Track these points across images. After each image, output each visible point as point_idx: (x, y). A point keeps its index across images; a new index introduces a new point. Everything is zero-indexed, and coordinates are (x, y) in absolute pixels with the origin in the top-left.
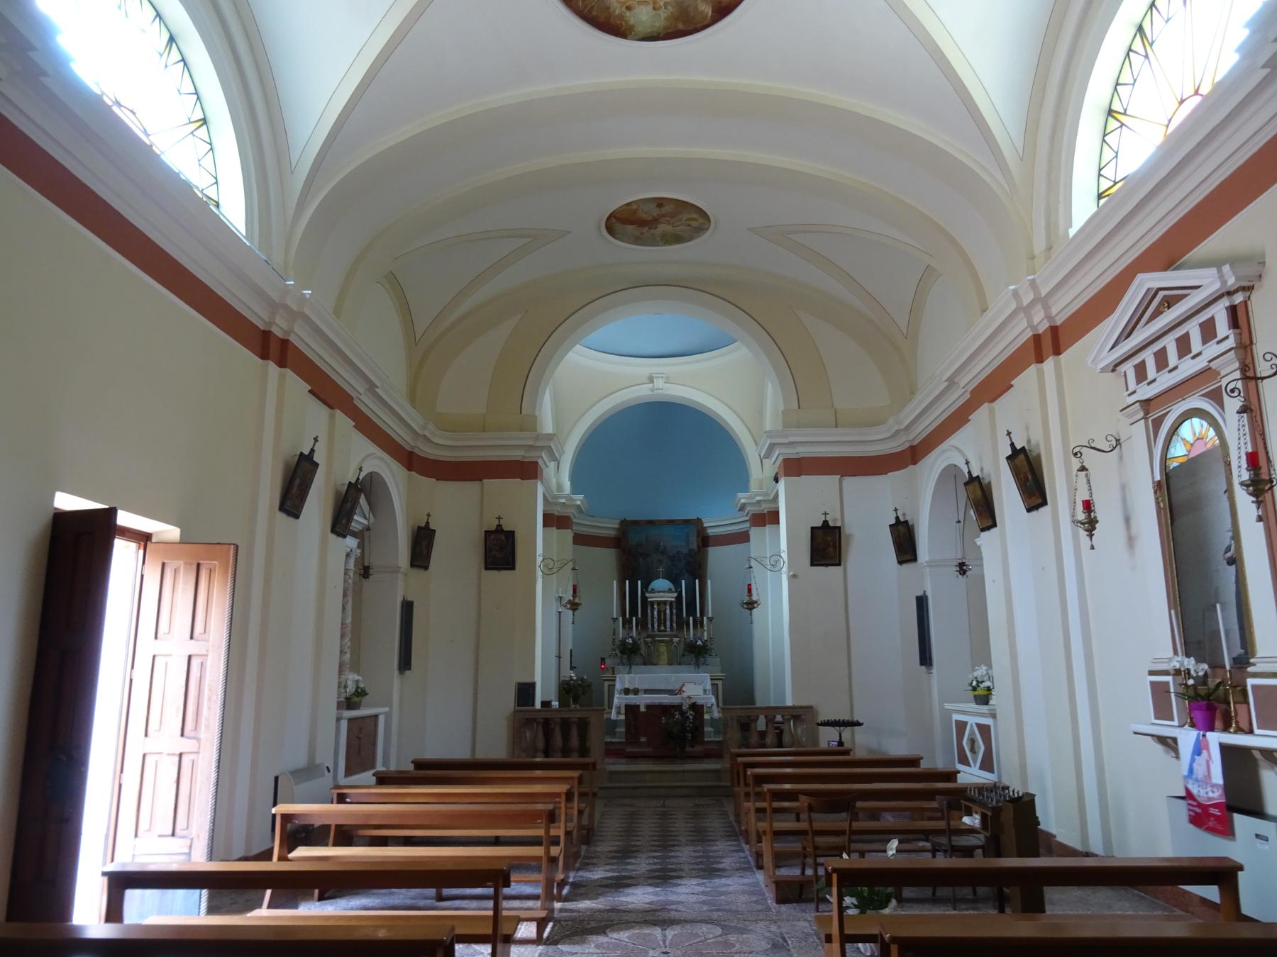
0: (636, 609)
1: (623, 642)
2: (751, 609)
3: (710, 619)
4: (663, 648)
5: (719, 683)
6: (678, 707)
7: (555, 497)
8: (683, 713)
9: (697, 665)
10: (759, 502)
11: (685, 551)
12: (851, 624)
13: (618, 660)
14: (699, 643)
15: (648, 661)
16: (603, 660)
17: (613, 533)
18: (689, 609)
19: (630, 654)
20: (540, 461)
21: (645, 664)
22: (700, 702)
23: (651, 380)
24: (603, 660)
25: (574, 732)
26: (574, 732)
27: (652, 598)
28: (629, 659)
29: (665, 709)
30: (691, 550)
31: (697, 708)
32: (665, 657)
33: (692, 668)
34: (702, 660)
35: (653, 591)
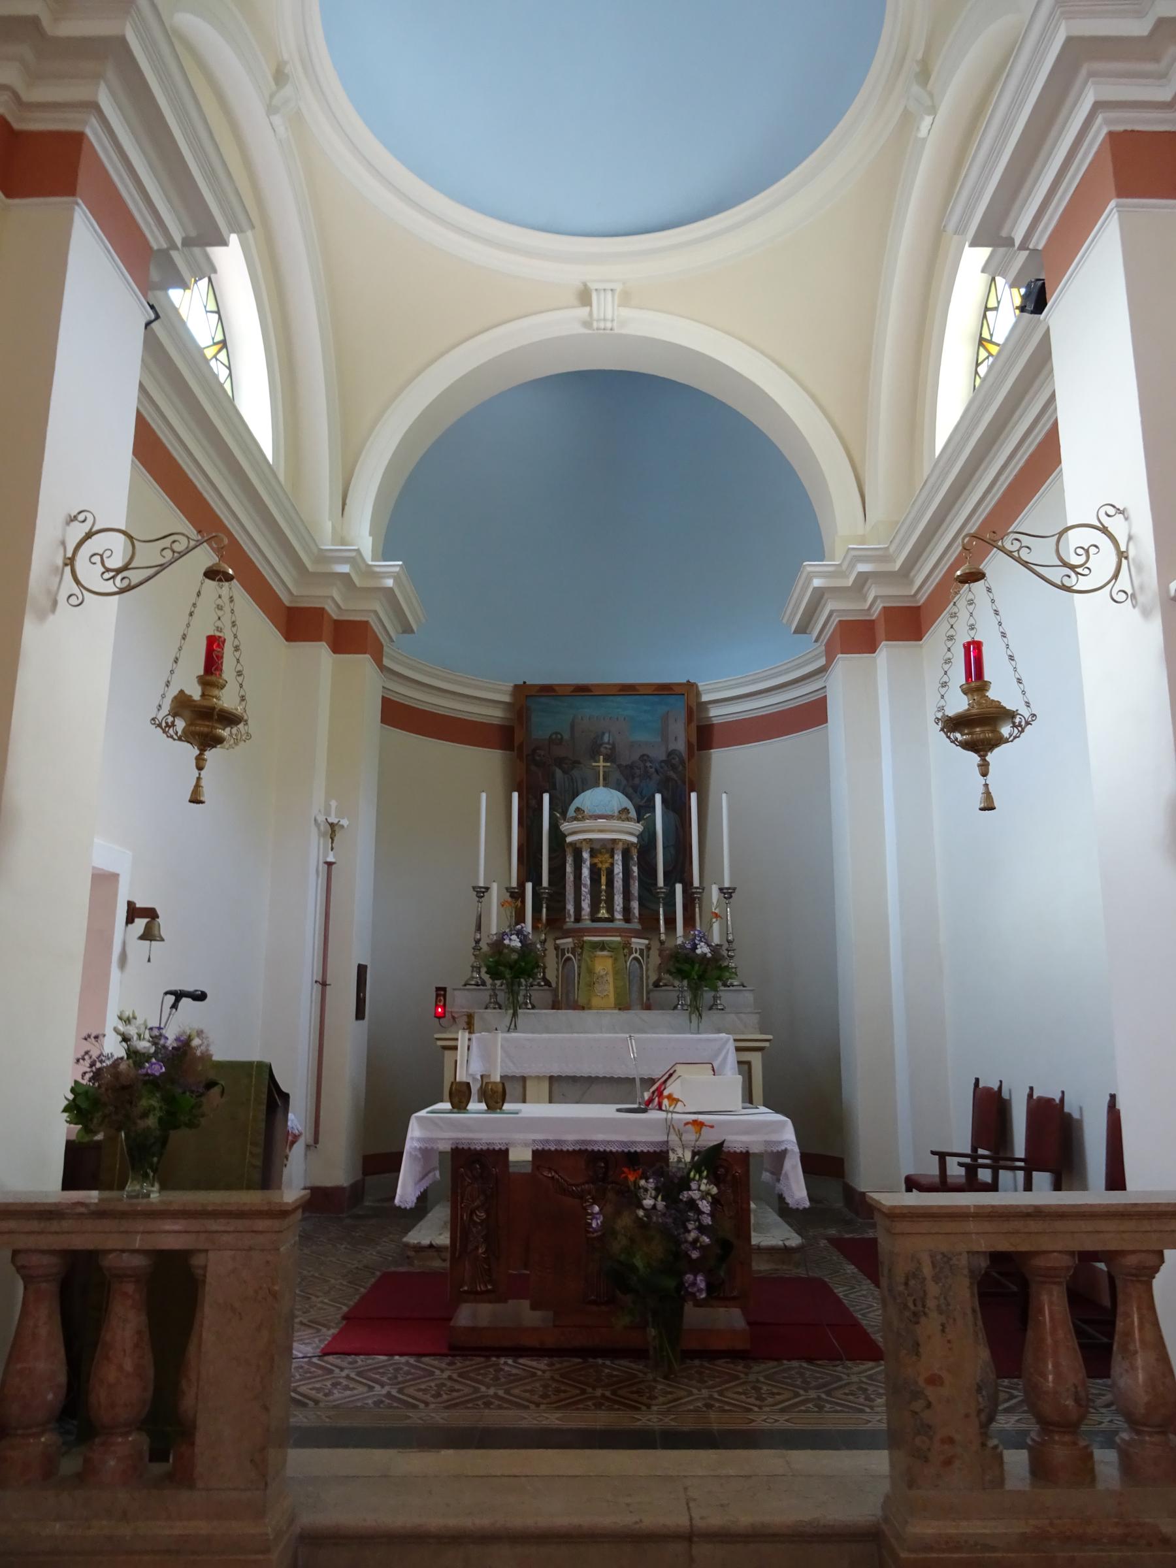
0: (543, 861)
1: (498, 946)
2: (981, 747)
3: (727, 893)
4: (603, 965)
5: (756, 1059)
6: (652, 1161)
7: (323, 557)
8: (673, 1186)
9: (696, 1009)
10: (863, 578)
11: (660, 754)
12: (322, 1114)
13: (485, 996)
14: (703, 949)
15: (564, 999)
16: (441, 992)
17: (495, 715)
18: (665, 871)
19: (512, 977)
20: (93, 132)
21: (555, 1006)
22: (737, 1142)
23: (585, 297)
24: (441, 992)
25: (125, 1327)
26: (125, 1327)
27: (576, 832)
28: (512, 992)
29: (605, 1171)
30: (671, 754)
31: (724, 1165)
32: (608, 989)
33: (680, 1017)
34: (707, 996)
35: (580, 815)
